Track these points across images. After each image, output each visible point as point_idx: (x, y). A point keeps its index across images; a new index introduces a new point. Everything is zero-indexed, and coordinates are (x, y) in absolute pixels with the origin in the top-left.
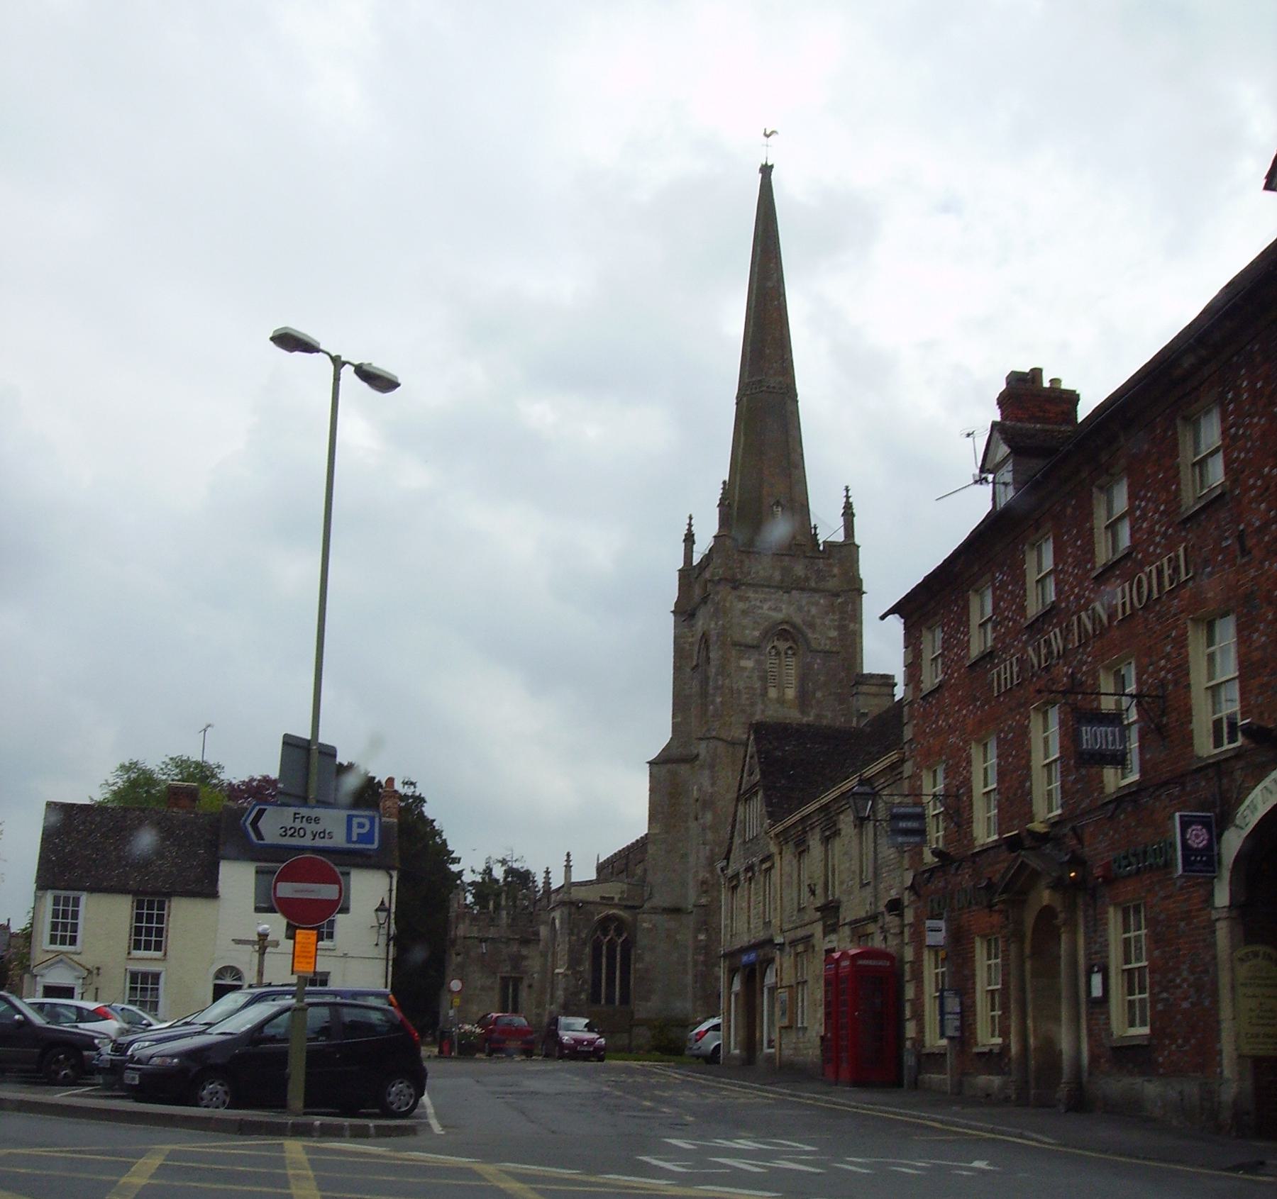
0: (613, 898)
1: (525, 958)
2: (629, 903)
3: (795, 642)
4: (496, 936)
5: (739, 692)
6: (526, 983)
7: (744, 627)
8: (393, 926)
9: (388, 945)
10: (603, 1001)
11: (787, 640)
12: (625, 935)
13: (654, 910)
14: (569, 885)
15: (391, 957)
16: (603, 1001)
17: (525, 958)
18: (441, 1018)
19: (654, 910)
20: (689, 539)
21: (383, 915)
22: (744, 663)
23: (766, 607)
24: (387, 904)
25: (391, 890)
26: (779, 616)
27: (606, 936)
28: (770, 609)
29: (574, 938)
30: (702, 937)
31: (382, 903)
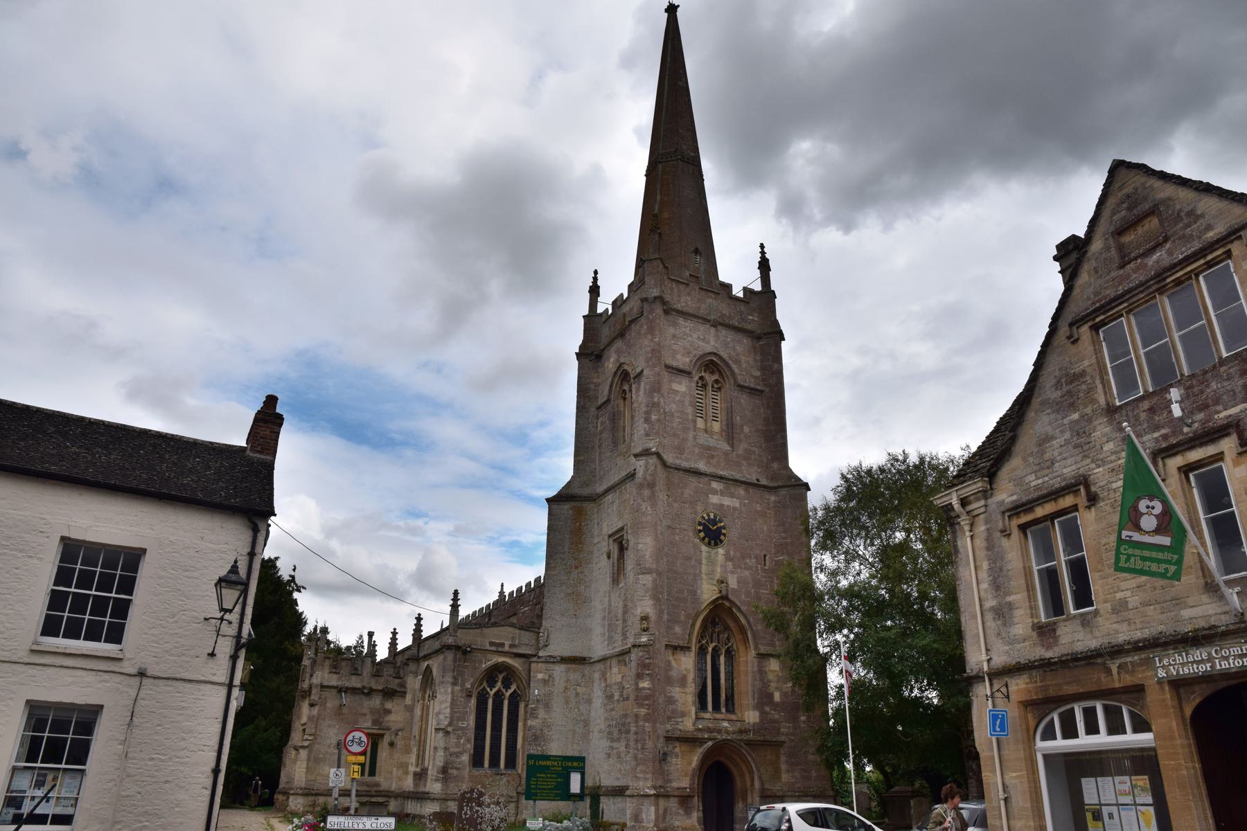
0: (502, 645)
1: (388, 712)
2: (520, 651)
3: (721, 374)
4: (359, 685)
5: (672, 415)
6: (387, 739)
7: (676, 352)
8: (247, 627)
9: (234, 658)
10: (486, 764)
11: (712, 373)
12: (513, 687)
13: (551, 660)
14: (456, 624)
15: (237, 681)
16: (486, 764)
17: (388, 712)
18: (283, 779)
19: (551, 660)
20: (594, 291)
21: (230, 596)
22: (675, 386)
23: (695, 336)
24: (243, 572)
25: (216, 772)
26: (709, 349)
27: (492, 687)
28: (699, 338)
29: (458, 688)
30: (645, 684)
31: (234, 569)
